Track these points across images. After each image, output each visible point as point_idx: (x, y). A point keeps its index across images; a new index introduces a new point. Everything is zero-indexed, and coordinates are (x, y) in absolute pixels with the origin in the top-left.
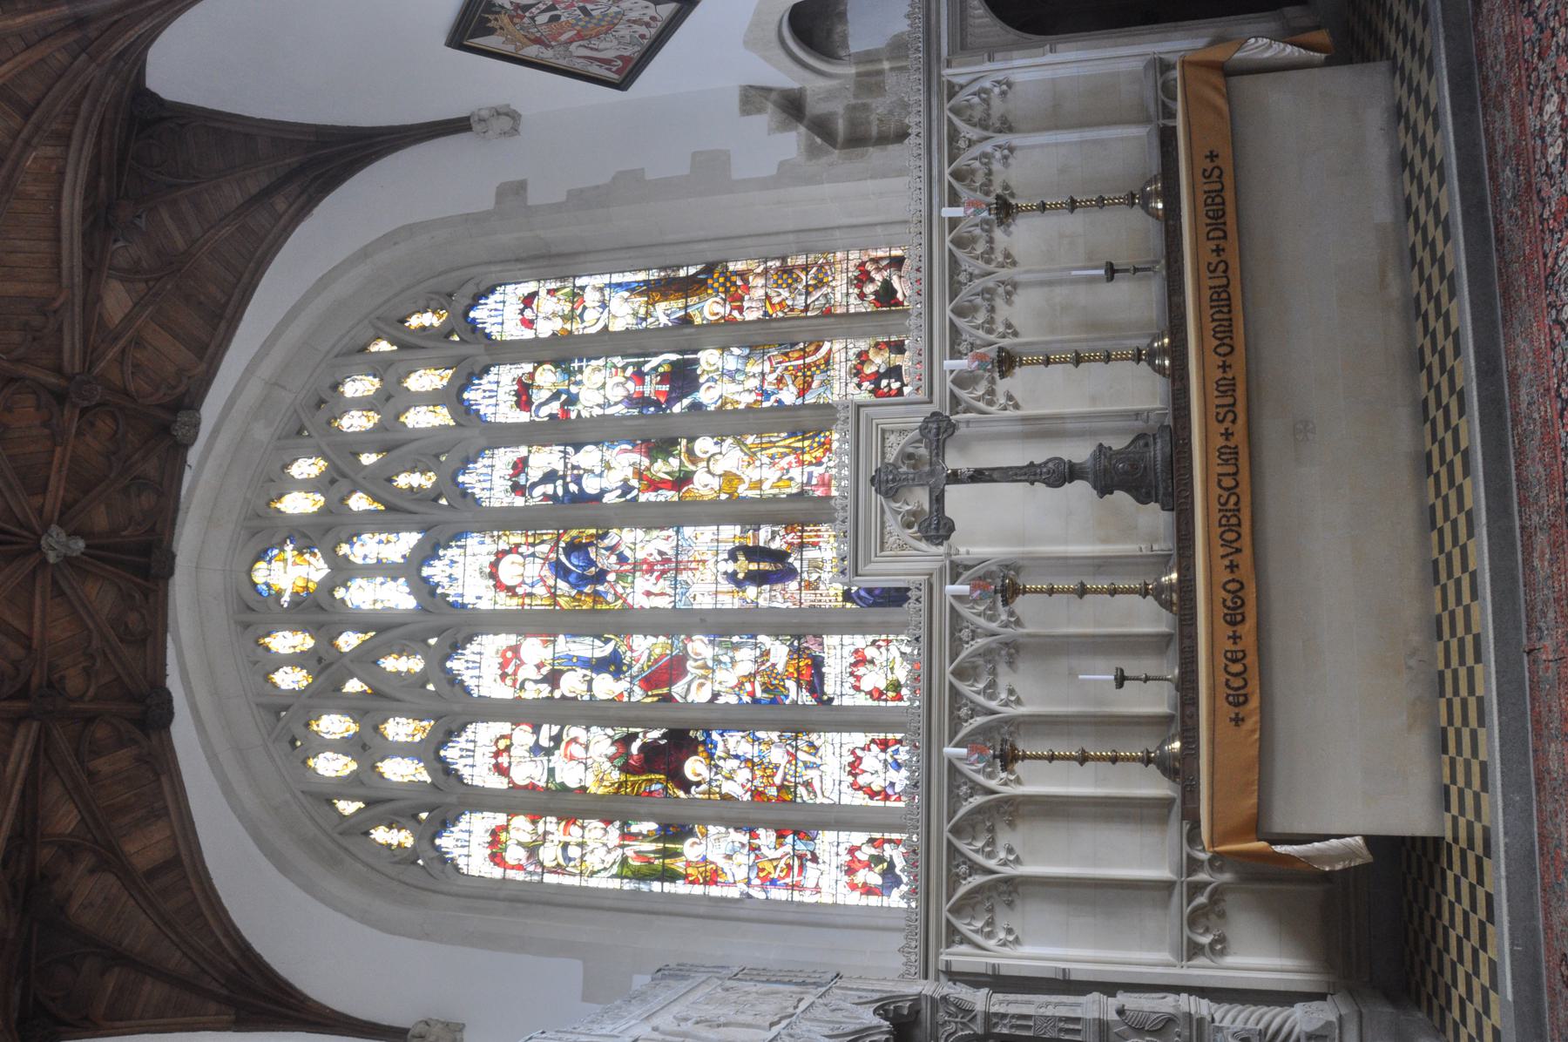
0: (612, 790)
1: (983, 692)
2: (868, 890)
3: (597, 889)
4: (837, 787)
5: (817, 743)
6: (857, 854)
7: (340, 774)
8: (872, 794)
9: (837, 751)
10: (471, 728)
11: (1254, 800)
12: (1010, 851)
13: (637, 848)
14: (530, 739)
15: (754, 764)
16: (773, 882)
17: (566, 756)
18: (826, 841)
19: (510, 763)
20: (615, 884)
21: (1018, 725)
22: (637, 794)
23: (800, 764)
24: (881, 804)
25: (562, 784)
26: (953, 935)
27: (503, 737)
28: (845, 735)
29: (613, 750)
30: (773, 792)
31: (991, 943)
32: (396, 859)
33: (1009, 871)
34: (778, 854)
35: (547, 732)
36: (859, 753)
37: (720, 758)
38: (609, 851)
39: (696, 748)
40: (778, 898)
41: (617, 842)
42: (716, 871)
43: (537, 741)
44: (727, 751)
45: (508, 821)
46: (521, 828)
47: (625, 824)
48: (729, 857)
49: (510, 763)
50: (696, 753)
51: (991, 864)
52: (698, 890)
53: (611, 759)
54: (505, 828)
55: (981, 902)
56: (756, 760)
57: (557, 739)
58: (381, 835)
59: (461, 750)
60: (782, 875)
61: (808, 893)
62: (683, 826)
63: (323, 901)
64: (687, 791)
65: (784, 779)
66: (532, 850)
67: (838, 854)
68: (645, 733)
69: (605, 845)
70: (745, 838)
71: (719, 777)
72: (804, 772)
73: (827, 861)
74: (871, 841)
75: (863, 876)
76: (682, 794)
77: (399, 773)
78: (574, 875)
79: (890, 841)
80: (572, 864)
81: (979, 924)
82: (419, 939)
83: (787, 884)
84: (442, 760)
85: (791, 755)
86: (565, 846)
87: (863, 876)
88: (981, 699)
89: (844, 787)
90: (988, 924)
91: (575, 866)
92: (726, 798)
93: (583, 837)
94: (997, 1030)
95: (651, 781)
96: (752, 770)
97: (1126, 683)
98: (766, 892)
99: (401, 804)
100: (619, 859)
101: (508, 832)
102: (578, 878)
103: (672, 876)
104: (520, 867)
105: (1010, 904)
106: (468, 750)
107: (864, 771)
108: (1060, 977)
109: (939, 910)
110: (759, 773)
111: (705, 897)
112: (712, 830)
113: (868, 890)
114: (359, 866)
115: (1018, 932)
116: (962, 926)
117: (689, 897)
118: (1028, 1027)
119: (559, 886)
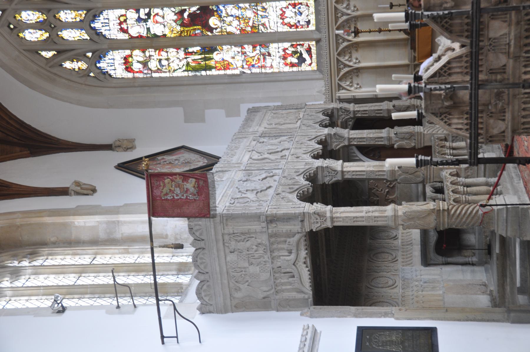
0: (177, 35)
1: (346, 8)
2: (292, 65)
3: (178, 77)
4: (276, 25)
5: (265, 7)
6: (287, 51)
7: (39, 39)
8: (291, 26)
9: (275, 9)
10: (105, 13)
11: (430, 47)
12: (357, 59)
13: (193, 58)
14: (136, 16)
15: (239, 18)
16: (253, 66)
17: (154, 22)
18: (273, 48)
19: (128, 27)
20: (186, 74)
21: (357, 19)
22: (190, 35)
23: (259, 16)
24: (295, 30)
25: (155, 34)
26: (340, 87)
27: (122, 16)
28: (277, 3)
29: (175, 17)
30: (249, 29)
31: (352, 89)
32: (81, 75)
33: (357, 66)
34: (254, 54)
35: (143, 13)
36: (284, 10)
37: (224, 17)
38: (180, 61)
39: (214, 14)
40: (256, 72)
41: (183, 56)
42: (228, 64)
43: (139, 16)
44: (227, 14)
45: (131, 52)
46: (138, 55)
47: (186, 49)
48: (233, 58)
49: (128, 27)
50: (214, 15)
51: (351, 64)
52: (222, 72)
53: (175, 21)
54: (131, 56)
55: (349, 76)
56: (240, 16)
57: (149, 15)
58: (68, 65)
59: (102, 23)
60: (257, 63)
61: (268, 69)
62: (212, 47)
63: (56, 98)
64: (212, 32)
65: (253, 23)
66: (145, 64)
67: (279, 52)
68: (189, 9)
69: (178, 58)
70: (239, 49)
71: (225, 25)
72: (261, 20)
73: (275, 55)
74: (292, 46)
75: (290, 60)
76: (209, 33)
77: (72, 36)
78: (166, 72)
79: (299, 45)
80: (164, 68)
81: (348, 83)
82: (108, 108)
83: (259, 66)
84: (94, 29)
85: (255, 13)
86: (160, 61)
87: (290, 60)
88: (345, 10)
89: (279, 24)
90: (351, 83)
91: (166, 69)
92: (229, 33)
93: (168, 56)
94: (357, 115)
95: (195, 29)
96: (239, 21)
97: (393, 7)
98: (251, 70)
99: (79, 51)
100: (185, 64)
101: (132, 58)
102: (168, 73)
103: (210, 68)
104: (140, 72)
105: (357, 76)
106: (105, 23)
107: (286, 17)
108: (375, 97)
109: (333, 29)
110: (242, 22)
111: (225, 75)
112: (225, 47)
113: (292, 65)
114: (64, 81)
115: (360, 84)
116: (343, 84)
117: (219, 76)
118: (367, 114)
119: (160, 77)
